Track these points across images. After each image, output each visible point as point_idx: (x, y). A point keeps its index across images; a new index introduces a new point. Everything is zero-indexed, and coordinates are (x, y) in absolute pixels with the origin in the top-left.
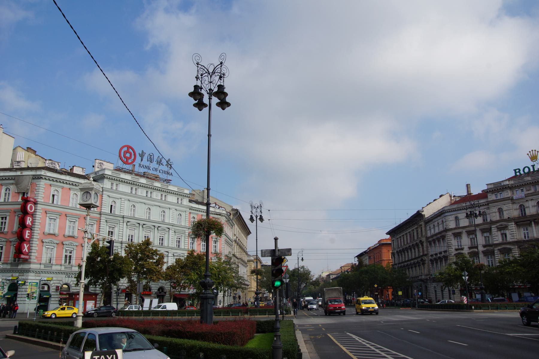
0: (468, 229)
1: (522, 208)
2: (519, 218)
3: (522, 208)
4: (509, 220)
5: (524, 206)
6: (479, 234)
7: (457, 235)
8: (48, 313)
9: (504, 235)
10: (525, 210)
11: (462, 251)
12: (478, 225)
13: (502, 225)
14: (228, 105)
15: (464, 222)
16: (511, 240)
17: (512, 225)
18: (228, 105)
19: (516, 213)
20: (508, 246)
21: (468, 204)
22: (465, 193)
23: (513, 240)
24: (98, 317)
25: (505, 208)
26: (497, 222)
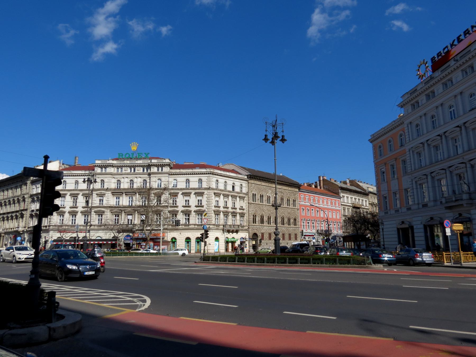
0: (216, 191)
1: (119, 182)
2: (115, 189)
3: (119, 182)
4: (107, 189)
5: (133, 181)
6: (180, 196)
7: (186, 194)
8: (317, 11)
9: (101, 201)
10: (133, 184)
11: (176, 209)
12: (81, 190)
13: (101, 193)
14: (285, 140)
15: (83, 186)
16: (106, 205)
17: (109, 194)
18: (285, 140)
19: (113, 185)
20: (103, 209)
21: (87, 172)
22: (73, 164)
23: (107, 205)
24: (446, 202)
25: (106, 180)
26: (184, 189)
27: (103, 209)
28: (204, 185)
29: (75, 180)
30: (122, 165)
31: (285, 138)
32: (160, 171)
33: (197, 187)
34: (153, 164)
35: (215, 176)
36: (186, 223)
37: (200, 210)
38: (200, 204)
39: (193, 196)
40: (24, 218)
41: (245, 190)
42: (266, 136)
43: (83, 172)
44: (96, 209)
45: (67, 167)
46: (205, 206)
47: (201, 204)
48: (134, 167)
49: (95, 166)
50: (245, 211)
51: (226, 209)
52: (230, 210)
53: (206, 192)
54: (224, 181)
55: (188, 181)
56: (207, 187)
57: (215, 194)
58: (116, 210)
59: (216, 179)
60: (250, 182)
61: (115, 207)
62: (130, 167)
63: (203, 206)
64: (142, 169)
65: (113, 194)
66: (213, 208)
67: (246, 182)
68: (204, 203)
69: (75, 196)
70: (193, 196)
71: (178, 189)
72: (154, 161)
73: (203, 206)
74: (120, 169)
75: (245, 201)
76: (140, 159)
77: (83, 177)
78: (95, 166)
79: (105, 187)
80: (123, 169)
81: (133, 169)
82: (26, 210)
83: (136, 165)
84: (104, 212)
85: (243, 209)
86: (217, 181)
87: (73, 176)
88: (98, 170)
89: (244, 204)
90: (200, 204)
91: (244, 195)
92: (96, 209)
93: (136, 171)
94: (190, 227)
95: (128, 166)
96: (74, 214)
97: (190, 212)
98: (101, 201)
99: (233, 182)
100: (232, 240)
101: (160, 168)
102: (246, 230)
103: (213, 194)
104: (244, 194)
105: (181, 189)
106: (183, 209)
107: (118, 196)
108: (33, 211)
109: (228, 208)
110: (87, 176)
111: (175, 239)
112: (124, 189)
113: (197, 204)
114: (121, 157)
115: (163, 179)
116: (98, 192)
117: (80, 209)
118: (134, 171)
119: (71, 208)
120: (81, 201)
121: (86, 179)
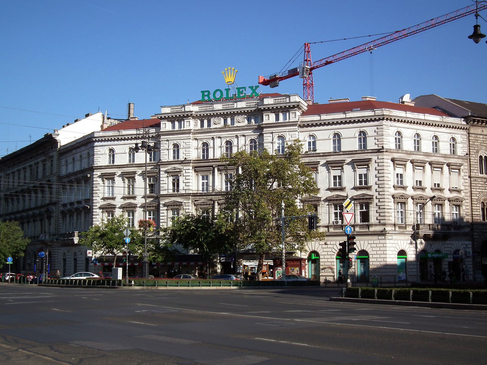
0: (396, 156)
2: (198, 161)
9: (176, 184)
11: (132, 201)
12: (140, 166)
13: (175, 168)
16: (184, 192)
20: (179, 199)
22: (126, 118)
25: (182, 144)
26: (329, 154)
27: (179, 199)
28: (371, 144)
29: (358, 130)
30: (208, 113)
31: (482, 31)
32: (177, 128)
33: (126, 162)
34: (266, 107)
35: (393, 123)
36: (337, 222)
37: (364, 195)
38: (364, 184)
39: (348, 169)
40: (53, 220)
41: (461, 150)
42: (476, 27)
43: (134, 132)
44: (167, 200)
45: (116, 122)
46: (375, 187)
47: (340, 184)
48: (232, 115)
49: (161, 118)
50: (462, 195)
51: (419, 192)
52: (410, 192)
53: (374, 157)
54: (413, 132)
55: (337, 137)
56: (376, 147)
57: (393, 160)
58: (203, 200)
59: (395, 130)
60: (472, 130)
61: (201, 195)
62: (225, 116)
63: (369, 188)
64: (222, 120)
65: (197, 170)
66: (393, 191)
67: (464, 132)
68: (372, 181)
69: (130, 177)
70: (348, 169)
71: (319, 155)
72: (218, 107)
73: (369, 188)
74: (177, 123)
75: (462, 174)
76: (242, 99)
77: (135, 141)
78: (161, 118)
79: (181, 158)
80: (236, 118)
81: (206, 122)
82: (55, 204)
83: (236, 111)
84: (180, 204)
85: (459, 191)
86: (112, 150)
87: (125, 139)
88: (166, 126)
89: (459, 181)
90: (364, 184)
91: (460, 161)
92: (167, 200)
93: (213, 126)
94: (372, 229)
95: (244, 113)
96: (130, 209)
97: (371, 198)
98: (176, 184)
99: (432, 134)
100: (435, 255)
101: (281, 115)
102: (465, 235)
103: (390, 161)
104: (459, 157)
105: (325, 155)
106: (330, 194)
107: (205, 174)
108: (65, 205)
109: (404, 188)
110: (141, 139)
111: (317, 254)
112: (214, 160)
113: (358, 184)
114: (206, 98)
115: (288, 137)
116: (170, 167)
117: (139, 201)
118: (209, 125)
119: (124, 198)
120: (141, 185)
121: (140, 145)
